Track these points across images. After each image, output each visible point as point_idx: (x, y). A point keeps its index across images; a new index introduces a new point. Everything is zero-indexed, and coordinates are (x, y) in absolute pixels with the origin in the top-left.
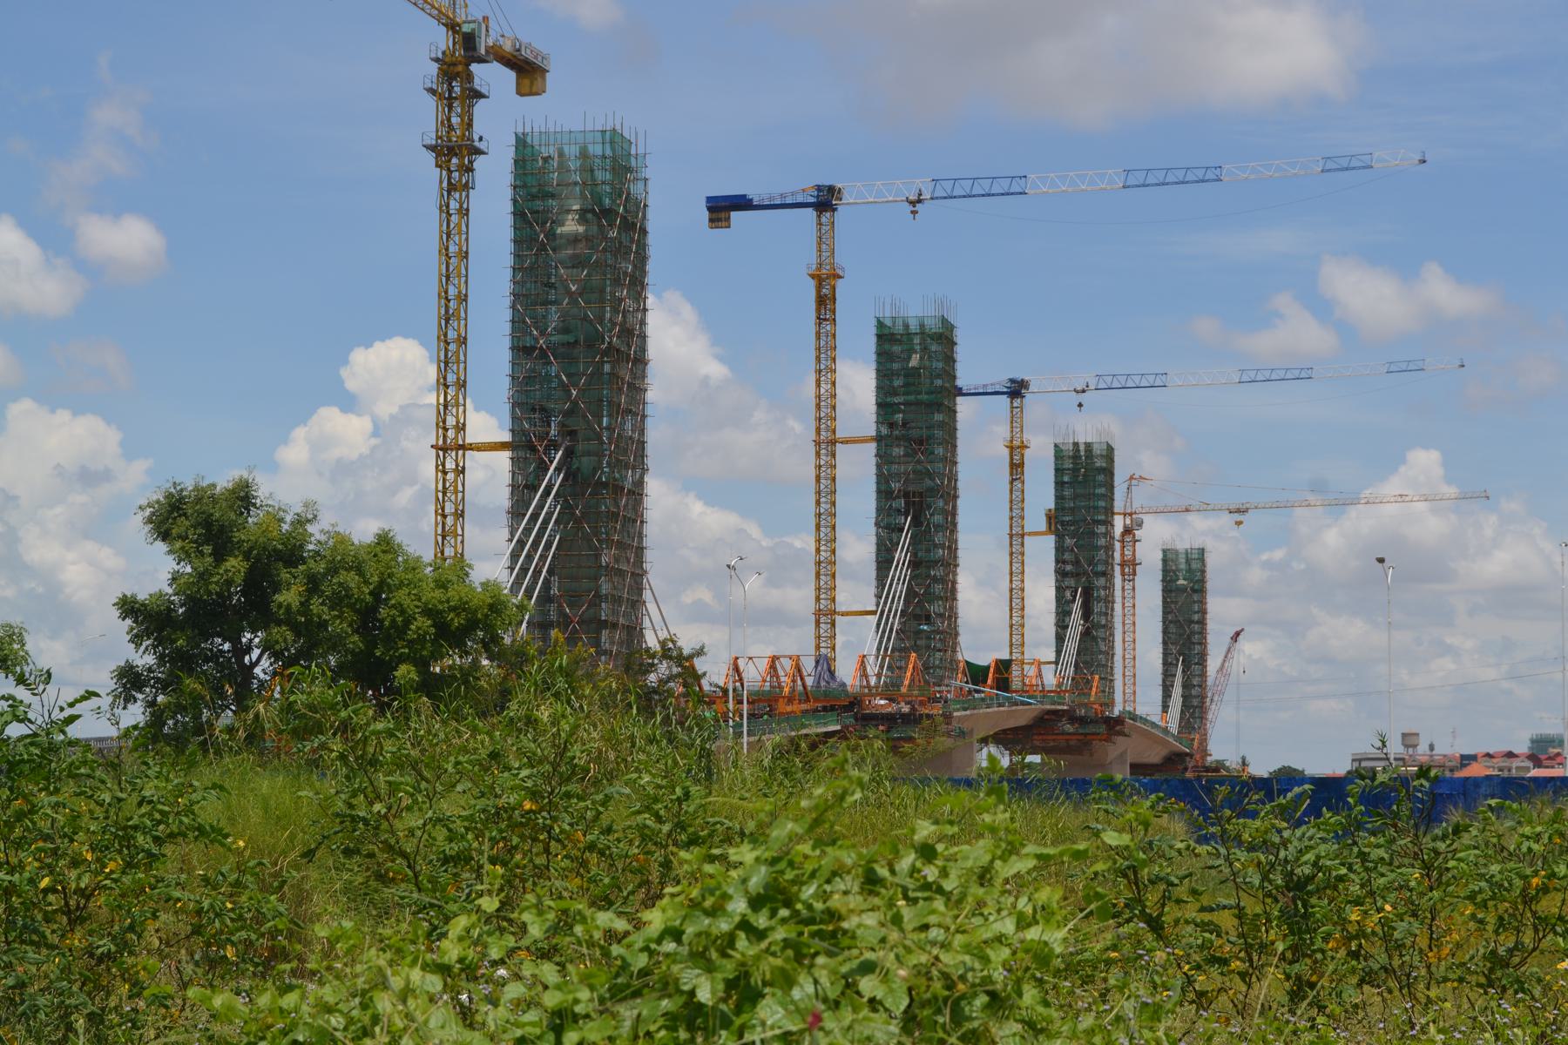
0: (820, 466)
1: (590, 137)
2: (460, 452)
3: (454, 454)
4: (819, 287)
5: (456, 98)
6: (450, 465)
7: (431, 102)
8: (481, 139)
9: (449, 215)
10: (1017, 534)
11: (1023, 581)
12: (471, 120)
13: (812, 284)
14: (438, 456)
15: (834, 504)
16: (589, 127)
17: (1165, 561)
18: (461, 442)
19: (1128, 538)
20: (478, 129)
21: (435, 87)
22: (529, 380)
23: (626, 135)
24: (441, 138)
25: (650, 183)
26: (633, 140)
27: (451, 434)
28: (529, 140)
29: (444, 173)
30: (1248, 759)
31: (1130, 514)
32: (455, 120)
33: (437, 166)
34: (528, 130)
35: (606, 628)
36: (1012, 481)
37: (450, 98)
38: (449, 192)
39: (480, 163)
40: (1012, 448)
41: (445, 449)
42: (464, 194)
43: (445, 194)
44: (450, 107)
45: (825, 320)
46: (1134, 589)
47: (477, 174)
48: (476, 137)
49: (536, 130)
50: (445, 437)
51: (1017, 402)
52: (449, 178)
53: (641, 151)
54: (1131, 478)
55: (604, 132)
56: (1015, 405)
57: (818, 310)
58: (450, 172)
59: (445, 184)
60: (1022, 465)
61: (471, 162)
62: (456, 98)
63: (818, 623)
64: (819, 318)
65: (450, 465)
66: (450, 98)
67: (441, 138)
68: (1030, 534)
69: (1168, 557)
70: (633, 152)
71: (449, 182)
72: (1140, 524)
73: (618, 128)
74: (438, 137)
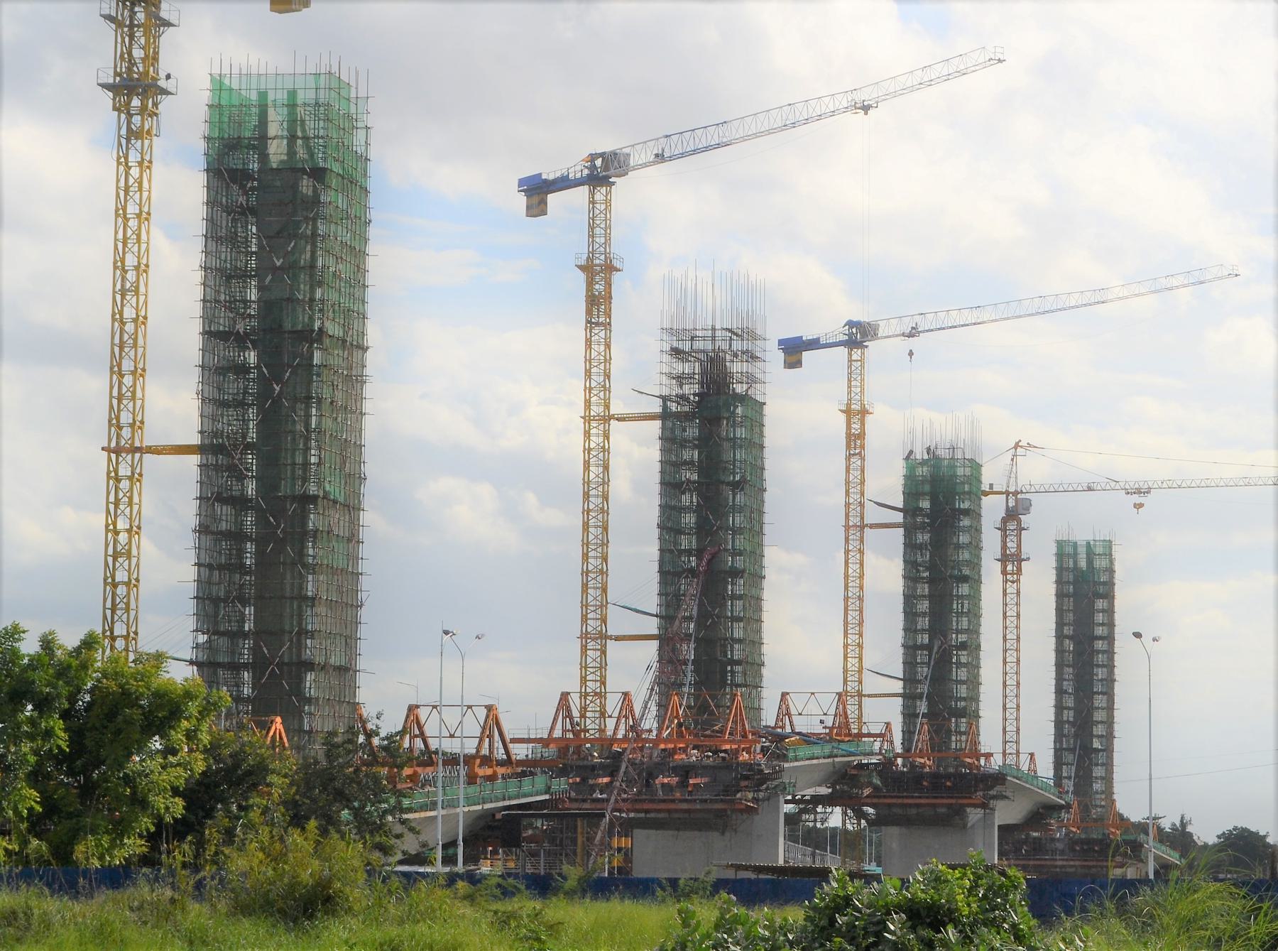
0: (589, 511)
1: (300, 84)
2: (137, 455)
3: (129, 457)
4: (590, 284)
5: (138, 26)
6: (124, 470)
7: (109, 29)
8: (168, 77)
9: (126, 219)
10: (855, 526)
11: (861, 635)
12: (156, 53)
13: (581, 277)
14: (110, 459)
15: (605, 559)
16: (300, 70)
17: (1060, 556)
18: (137, 444)
19: (1012, 526)
20: (164, 65)
21: (114, 14)
22: (209, 583)
23: (344, 77)
24: (120, 75)
25: (372, 132)
26: (353, 83)
27: (126, 433)
28: (227, 82)
29: (123, 116)
30: (1187, 818)
31: (1016, 493)
32: (138, 53)
33: (115, 109)
34: (226, 71)
35: (312, 670)
36: (849, 457)
37: (131, 26)
38: (128, 140)
39: (165, 104)
40: (848, 412)
41: (118, 451)
42: (147, 142)
43: (124, 142)
44: (132, 37)
45: (597, 324)
46: (1018, 593)
47: (162, 118)
48: (162, 75)
49: (235, 71)
50: (119, 436)
51: (856, 354)
52: (129, 123)
53: (362, 94)
54: (1017, 446)
55: (317, 75)
56: (854, 357)
57: (589, 312)
58: (130, 115)
59: (123, 131)
60: (862, 436)
61: (156, 105)
62: (138, 26)
63: (584, 649)
64: (588, 322)
65: (124, 470)
66: (131, 26)
67: (120, 75)
68: (872, 526)
69: (1064, 553)
70: (353, 95)
71: (129, 129)
72: (1027, 510)
73: (335, 69)
74: (116, 74)
